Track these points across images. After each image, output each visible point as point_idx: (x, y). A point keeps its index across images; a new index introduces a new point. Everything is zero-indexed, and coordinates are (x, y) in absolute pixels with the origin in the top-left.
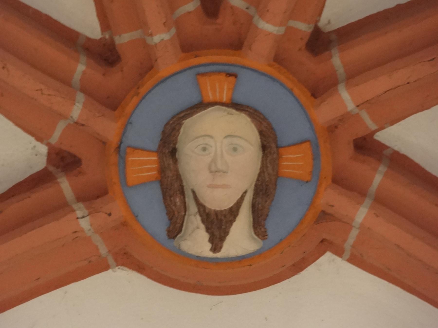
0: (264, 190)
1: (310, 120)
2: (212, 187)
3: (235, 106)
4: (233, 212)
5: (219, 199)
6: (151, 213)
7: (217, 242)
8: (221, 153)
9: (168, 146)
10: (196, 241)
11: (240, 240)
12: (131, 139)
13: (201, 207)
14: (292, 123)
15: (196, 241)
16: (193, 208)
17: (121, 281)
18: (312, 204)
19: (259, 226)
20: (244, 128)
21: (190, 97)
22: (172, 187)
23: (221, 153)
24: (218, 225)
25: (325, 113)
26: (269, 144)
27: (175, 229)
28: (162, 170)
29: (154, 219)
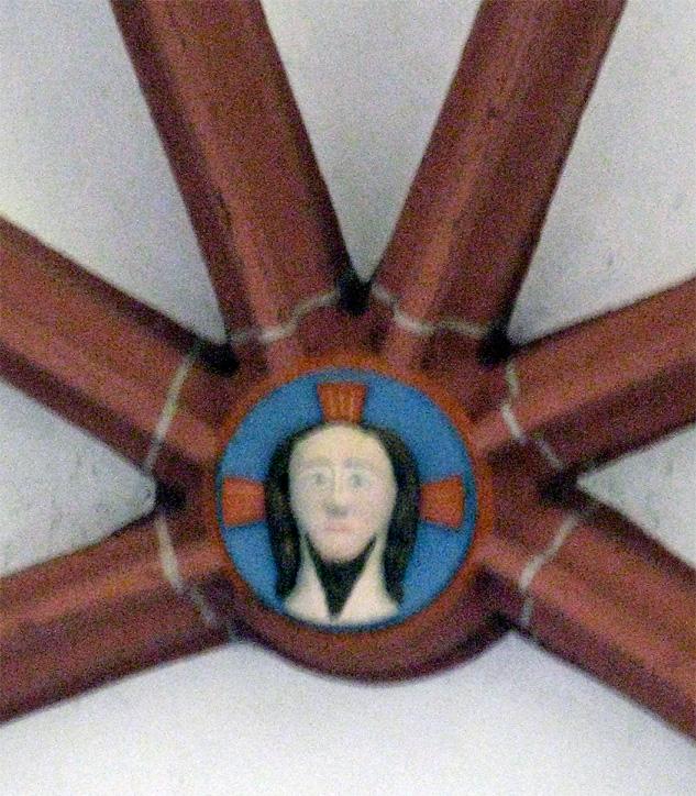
0: (401, 537)
1: (465, 444)
2: (329, 529)
3: (364, 424)
4: (356, 566)
5: (339, 544)
6: (253, 560)
7: (336, 602)
8: (345, 484)
9: (278, 476)
10: (310, 602)
11: (368, 602)
12: (230, 464)
13: (312, 549)
14: (443, 457)
15: (310, 602)
16: (306, 554)
17: (237, 672)
18: (463, 560)
19: (393, 580)
20: (370, 450)
21: (304, 410)
22: (283, 530)
23: (345, 484)
24: (338, 579)
25: (484, 439)
26: (405, 469)
27: (287, 582)
28: (268, 506)
29: (258, 572)
